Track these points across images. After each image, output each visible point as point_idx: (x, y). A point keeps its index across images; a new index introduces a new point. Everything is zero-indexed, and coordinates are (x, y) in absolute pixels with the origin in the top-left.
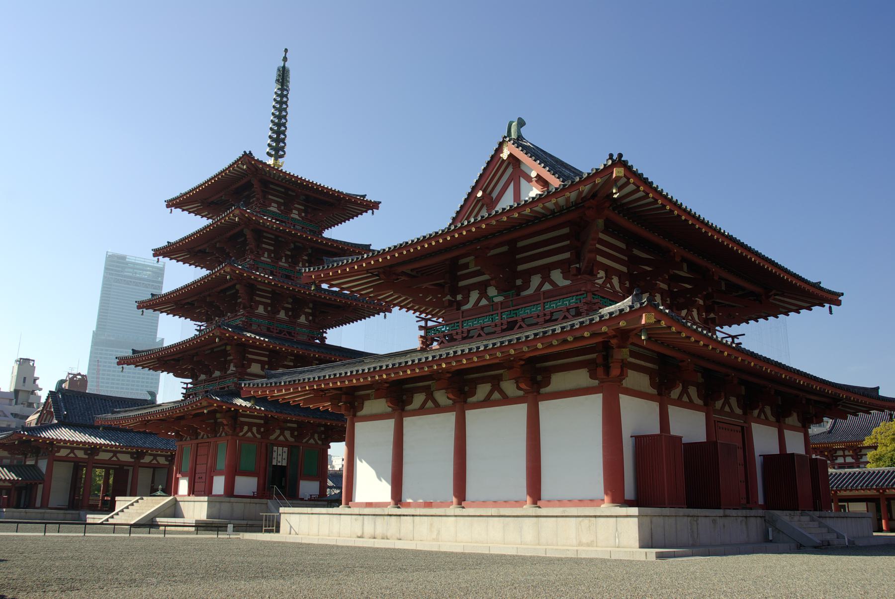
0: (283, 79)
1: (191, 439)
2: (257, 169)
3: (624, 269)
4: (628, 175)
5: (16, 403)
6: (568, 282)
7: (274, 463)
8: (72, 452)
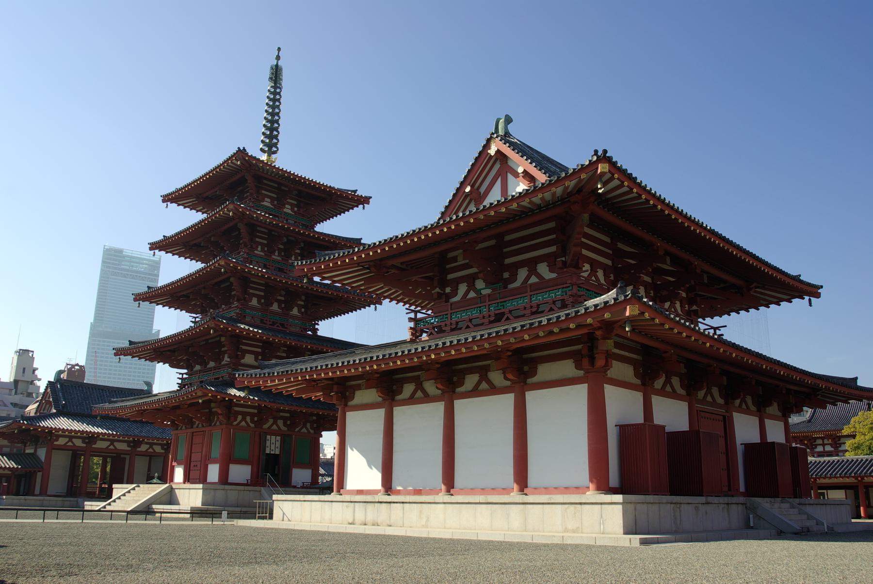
0: (276, 77)
1: (186, 428)
2: (250, 164)
3: (609, 262)
4: (613, 171)
5: (16, 393)
6: (554, 275)
7: (268, 451)
8: (70, 440)
